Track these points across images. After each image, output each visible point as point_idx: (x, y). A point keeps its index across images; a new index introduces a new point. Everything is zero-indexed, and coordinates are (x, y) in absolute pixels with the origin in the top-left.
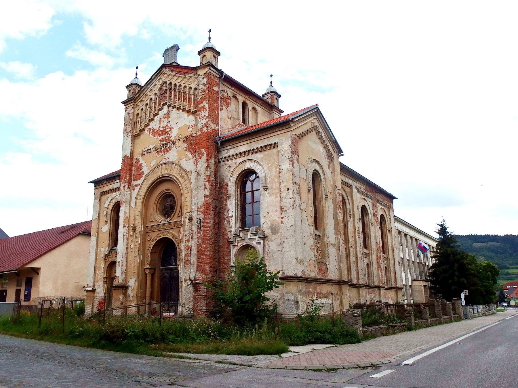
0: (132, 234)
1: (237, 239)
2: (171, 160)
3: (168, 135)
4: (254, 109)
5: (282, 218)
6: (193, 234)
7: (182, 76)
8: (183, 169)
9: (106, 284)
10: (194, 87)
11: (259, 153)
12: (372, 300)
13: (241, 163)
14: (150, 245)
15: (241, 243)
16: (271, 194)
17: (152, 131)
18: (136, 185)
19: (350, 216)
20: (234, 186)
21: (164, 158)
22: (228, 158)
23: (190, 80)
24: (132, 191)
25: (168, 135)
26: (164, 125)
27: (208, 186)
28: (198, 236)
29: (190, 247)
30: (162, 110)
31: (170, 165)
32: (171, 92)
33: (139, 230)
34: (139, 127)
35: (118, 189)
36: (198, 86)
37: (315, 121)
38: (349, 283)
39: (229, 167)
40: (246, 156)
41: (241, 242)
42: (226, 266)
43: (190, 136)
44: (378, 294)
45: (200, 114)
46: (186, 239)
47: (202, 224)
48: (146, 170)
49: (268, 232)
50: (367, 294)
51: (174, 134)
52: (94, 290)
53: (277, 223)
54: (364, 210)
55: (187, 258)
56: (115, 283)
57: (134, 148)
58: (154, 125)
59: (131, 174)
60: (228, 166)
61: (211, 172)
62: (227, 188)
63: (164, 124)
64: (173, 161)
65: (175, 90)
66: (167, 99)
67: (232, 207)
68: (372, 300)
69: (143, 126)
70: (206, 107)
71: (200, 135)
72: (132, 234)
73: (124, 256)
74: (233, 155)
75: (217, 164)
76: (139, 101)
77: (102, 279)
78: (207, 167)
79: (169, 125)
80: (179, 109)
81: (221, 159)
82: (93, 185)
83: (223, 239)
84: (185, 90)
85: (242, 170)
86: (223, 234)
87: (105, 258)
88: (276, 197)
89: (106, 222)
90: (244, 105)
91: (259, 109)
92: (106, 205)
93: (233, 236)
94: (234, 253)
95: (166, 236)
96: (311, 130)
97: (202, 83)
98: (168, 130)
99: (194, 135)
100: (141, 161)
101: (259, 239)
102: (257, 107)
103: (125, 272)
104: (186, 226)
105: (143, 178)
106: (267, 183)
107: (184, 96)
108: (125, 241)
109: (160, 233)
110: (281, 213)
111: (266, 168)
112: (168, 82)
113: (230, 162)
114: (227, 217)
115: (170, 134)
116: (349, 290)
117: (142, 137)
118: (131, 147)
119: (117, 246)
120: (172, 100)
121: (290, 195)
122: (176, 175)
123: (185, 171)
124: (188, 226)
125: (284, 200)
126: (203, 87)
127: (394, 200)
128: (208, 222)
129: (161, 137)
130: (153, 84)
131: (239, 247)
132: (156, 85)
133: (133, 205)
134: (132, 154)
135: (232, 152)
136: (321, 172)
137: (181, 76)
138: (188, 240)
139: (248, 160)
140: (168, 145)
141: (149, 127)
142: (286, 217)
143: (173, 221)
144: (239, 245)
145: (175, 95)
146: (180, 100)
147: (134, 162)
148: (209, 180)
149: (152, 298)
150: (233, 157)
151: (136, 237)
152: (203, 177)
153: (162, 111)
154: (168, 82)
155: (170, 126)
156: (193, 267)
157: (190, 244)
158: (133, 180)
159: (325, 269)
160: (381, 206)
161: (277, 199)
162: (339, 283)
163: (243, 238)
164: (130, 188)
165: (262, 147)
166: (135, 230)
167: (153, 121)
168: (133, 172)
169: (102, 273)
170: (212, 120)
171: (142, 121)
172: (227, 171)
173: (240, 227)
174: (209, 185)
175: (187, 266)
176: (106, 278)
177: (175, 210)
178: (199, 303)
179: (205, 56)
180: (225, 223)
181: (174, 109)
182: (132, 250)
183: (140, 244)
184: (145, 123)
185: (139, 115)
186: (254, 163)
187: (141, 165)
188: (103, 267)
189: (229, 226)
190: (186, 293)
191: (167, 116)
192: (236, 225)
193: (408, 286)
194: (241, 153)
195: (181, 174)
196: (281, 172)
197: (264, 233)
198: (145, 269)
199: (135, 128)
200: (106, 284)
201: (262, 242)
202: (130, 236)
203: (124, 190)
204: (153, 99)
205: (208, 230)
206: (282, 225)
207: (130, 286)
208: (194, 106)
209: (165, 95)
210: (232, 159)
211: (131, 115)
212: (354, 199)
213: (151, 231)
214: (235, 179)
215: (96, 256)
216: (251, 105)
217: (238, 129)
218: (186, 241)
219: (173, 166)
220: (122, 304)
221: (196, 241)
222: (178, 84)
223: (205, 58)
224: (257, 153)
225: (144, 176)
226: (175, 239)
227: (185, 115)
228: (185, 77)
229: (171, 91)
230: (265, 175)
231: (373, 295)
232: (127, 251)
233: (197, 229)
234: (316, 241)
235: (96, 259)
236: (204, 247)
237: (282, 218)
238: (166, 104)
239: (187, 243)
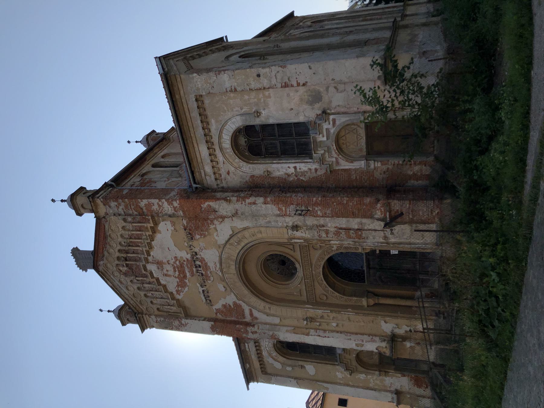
0: (318, 324)
1: (328, 159)
2: (217, 259)
5: (298, 84)
6: (318, 224)
7: (108, 240)
8: (229, 239)
9: (388, 372)
10: (123, 222)
11: (210, 127)
14: (335, 297)
15: (333, 153)
16: (266, 106)
17: (180, 289)
18: (251, 314)
21: (214, 270)
22: (217, 175)
23: (113, 229)
24: (258, 321)
25: (185, 263)
26: (172, 270)
27: (252, 199)
29: (336, 229)
30: (152, 273)
31: (223, 260)
33: (312, 312)
34: (174, 309)
35: (257, 343)
36: (120, 215)
39: (228, 173)
40: (213, 147)
41: (331, 152)
43: (185, 230)
47: (303, 208)
48: (231, 299)
51: (185, 255)
52: (398, 393)
53: (306, 94)
55: (352, 235)
57: (201, 317)
58: (172, 286)
61: (233, 196)
63: (169, 268)
66: (138, 263)
67: (282, 168)
69: (173, 301)
70: (147, 203)
71: (183, 211)
72: (318, 324)
73: (349, 337)
74: (213, 167)
75: (224, 190)
76: (141, 307)
77: (381, 377)
78: (225, 199)
79: (172, 262)
80: (151, 246)
81: (217, 185)
82: (252, 385)
84: (127, 236)
85: (232, 153)
88: (269, 97)
89: (302, 367)
91: (165, 151)
92: (278, 366)
93: (323, 164)
94: (347, 163)
98: (178, 263)
99: (185, 222)
100: (218, 306)
101: (327, 122)
102: (162, 154)
103: (371, 337)
104: (307, 235)
105: (241, 302)
106: (250, 112)
107: (135, 239)
108: (327, 334)
110: (292, 86)
111: (230, 114)
112: (117, 262)
113: (223, 172)
114: (296, 177)
115: (184, 261)
117: (187, 303)
118: (199, 320)
119: (334, 349)
120: (139, 256)
121: (266, 72)
122: (238, 251)
123: (231, 236)
124: (307, 232)
125: (274, 81)
126: (121, 207)
127: (295, 15)
128: (301, 200)
129: (188, 274)
130: (119, 284)
131: (338, 155)
132: (120, 282)
133: (277, 321)
134: (209, 320)
135: (208, 169)
137: (109, 243)
138: (327, 232)
140: (198, 263)
141: (175, 293)
142: (297, 78)
143: (299, 258)
144: (335, 156)
145: (134, 253)
146: (140, 244)
147: (219, 316)
148: (244, 199)
149: (411, 298)
150: (219, 179)
151: (322, 317)
152: (238, 206)
153: (154, 272)
155: (174, 260)
156: (365, 224)
157: (332, 230)
158: (244, 320)
161: (272, 95)
163: (326, 149)
164: (255, 324)
165: (202, 122)
166: (311, 318)
167: (167, 286)
168: (233, 319)
169: (374, 378)
170: (165, 195)
171: (167, 304)
172: (234, 176)
174: (251, 198)
175: (364, 235)
176: (380, 371)
178: (421, 213)
179: (82, 206)
180: (304, 179)
181: (152, 253)
182: (340, 325)
183: (331, 311)
184: (162, 292)
185: (159, 307)
186: (223, 135)
187: (224, 306)
188: (364, 375)
189: (309, 173)
190: (405, 237)
191: (160, 264)
192: (307, 162)
194: (210, 155)
195: (236, 244)
196: (235, 88)
197: (320, 115)
198: (368, 306)
199: (176, 314)
200: (388, 372)
201: (331, 117)
202: (320, 327)
203: (256, 332)
204: (139, 285)
205: (313, 200)
206: (309, 84)
207: (393, 330)
209: (134, 268)
210: (219, 168)
211: (159, 319)
213: (312, 286)
214: (245, 164)
215: (348, 385)
216: (157, 159)
217: (184, 172)
218: (327, 237)
219: (224, 256)
220: (418, 344)
221: (327, 219)
222: (119, 247)
223: (84, 206)
225: (238, 302)
226: (325, 255)
227: (158, 236)
228: (110, 236)
230: (240, 115)
232: (341, 333)
235: (353, 386)
236: (337, 204)
237: (298, 84)
238: (145, 266)
239: (331, 235)
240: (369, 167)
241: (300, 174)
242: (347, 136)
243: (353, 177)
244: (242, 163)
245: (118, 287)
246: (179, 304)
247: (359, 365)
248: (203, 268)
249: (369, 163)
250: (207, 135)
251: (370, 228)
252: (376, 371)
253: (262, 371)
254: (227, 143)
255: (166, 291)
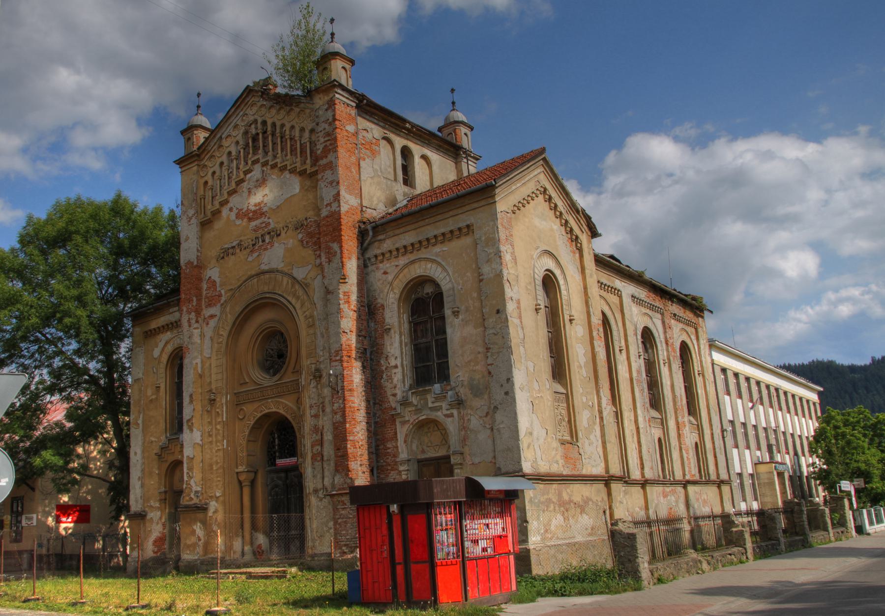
2: (274, 265)
3: (266, 220)
4: (424, 157)
9: (165, 503)
12: (671, 509)
13: (406, 265)
18: (212, 316)
19: (620, 351)
20: (396, 309)
28: (335, 408)
29: (321, 427)
30: (250, 172)
32: (265, 139)
37: (542, 176)
38: (625, 479)
39: (385, 273)
42: (390, 460)
44: (651, 512)
45: (324, 178)
46: (312, 414)
49: (463, 392)
50: (662, 498)
54: (647, 336)
56: (184, 501)
59: (201, 295)
60: (382, 271)
62: (383, 314)
64: (279, 267)
65: (273, 134)
68: (671, 509)
81: (369, 259)
83: (381, 409)
84: (293, 134)
85: (409, 278)
86: (380, 401)
87: (159, 456)
90: (406, 153)
95: (274, 410)
96: (534, 195)
97: (322, 119)
107: (291, 146)
109: (263, 404)
112: (260, 120)
113: (385, 266)
114: (386, 369)
116: (626, 493)
126: (326, 126)
129: (253, 224)
130: (232, 124)
131: (412, 423)
135: (388, 245)
136: (557, 272)
139: (420, 260)
145: (274, 144)
154: (260, 120)
156: (329, 465)
157: (320, 423)
158: (204, 307)
159: (577, 455)
160: (681, 326)
162: (607, 480)
163: (419, 407)
165: (443, 234)
173: (411, 388)
175: (317, 463)
176: (165, 492)
177: (287, 359)
192: (404, 382)
193: (745, 475)
200: (165, 503)
203: (190, 326)
204: (234, 153)
208: (311, 162)
212: (627, 316)
214: (397, 296)
216: (417, 150)
221: (331, 416)
222: (278, 124)
224: (435, 245)
229: (266, 135)
231: (673, 498)
233: (332, 394)
234: (557, 404)
240: (401, 464)
241: (389, 374)
242: (439, 433)
243: (389, 445)
244: (397, 291)
245: (229, 121)
246: (217, 213)
247: (169, 465)
248: (262, 245)
249: (405, 463)
250: (428, 242)
251: (326, 470)
252: (165, 487)
253: (146, 332)
254: (419, 270)
255: (232, 193)
